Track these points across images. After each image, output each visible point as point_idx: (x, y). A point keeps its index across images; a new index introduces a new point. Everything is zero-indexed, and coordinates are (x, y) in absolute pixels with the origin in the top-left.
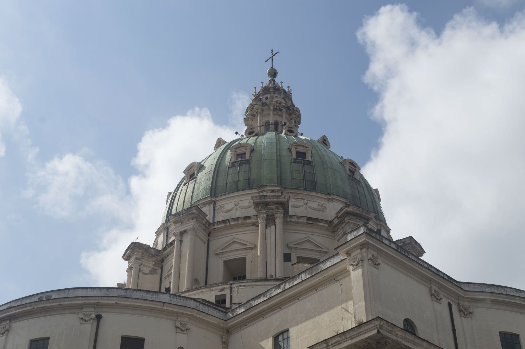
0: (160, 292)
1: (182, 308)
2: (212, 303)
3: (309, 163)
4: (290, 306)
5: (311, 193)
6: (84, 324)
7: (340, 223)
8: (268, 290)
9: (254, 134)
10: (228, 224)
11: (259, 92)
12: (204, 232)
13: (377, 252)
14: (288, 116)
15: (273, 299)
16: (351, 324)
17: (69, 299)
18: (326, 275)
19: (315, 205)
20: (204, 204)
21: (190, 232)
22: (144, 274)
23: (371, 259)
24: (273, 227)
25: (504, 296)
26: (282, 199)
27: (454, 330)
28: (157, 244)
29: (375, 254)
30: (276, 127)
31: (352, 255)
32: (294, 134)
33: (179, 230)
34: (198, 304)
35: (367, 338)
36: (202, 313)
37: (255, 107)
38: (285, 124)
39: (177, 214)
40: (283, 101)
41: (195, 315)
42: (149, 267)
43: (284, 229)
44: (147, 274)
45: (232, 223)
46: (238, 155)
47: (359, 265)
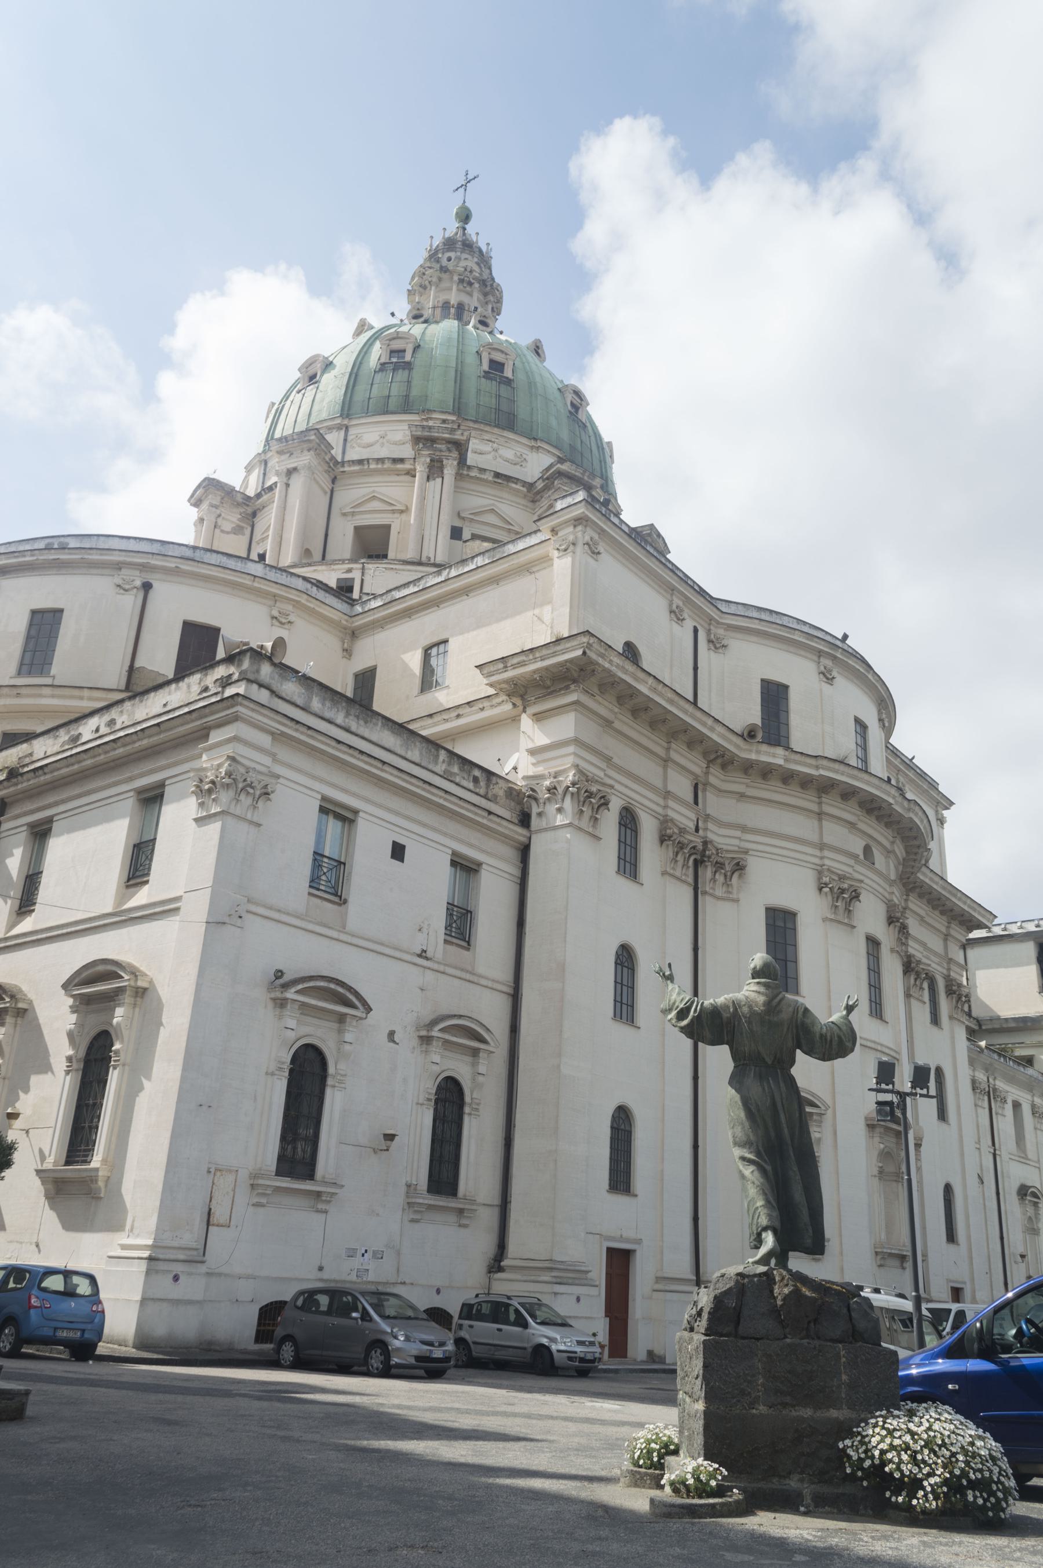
0: (248, 558)
1: (284, 588)
2: (332, 588)
3: (509, 382)
4: (453, 604)
5: (506, 434)
6: (123, 594)
7: (546, 488)
8: (422, 577)
9: (422, 319)
10: (366, 467)
11: (438, 246)
12: (326, 476)
13: (599, 534)
14: (481, 297)
15: (428, 590)
16: (544, 637)
17: (99, 552)
18: (515, 562)
19: (509, 454)
20: (330, 429)
21: (302, 472)
22: (222, 531)
23: (587, 544)
24: (439, 480)
25: (779, 627)
26: (457, 436)
27: (696, 668)
28: (246, 487)
29: (596, 537)
30: (460, 313)
31: (560, 534)
32: (489, 330)
33: (284, 467)
34: (309, 586)
35: (566, 661)
36: (314, 601)
37: (429, 272)
38: (476, 309)
39: (284, 439)
40: (476, 268)
41: (303, 601)
42: (233, 522)
43: (456, 487)
44: (228, 533)
45: (373, 466)
46: (392, 352)
47: (568, 551)
